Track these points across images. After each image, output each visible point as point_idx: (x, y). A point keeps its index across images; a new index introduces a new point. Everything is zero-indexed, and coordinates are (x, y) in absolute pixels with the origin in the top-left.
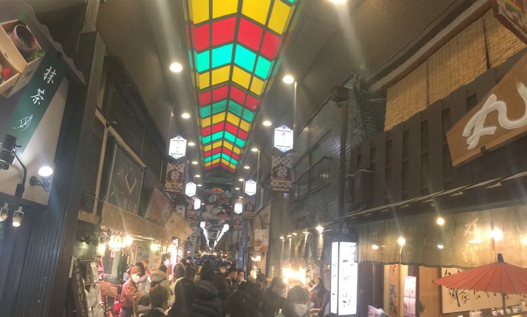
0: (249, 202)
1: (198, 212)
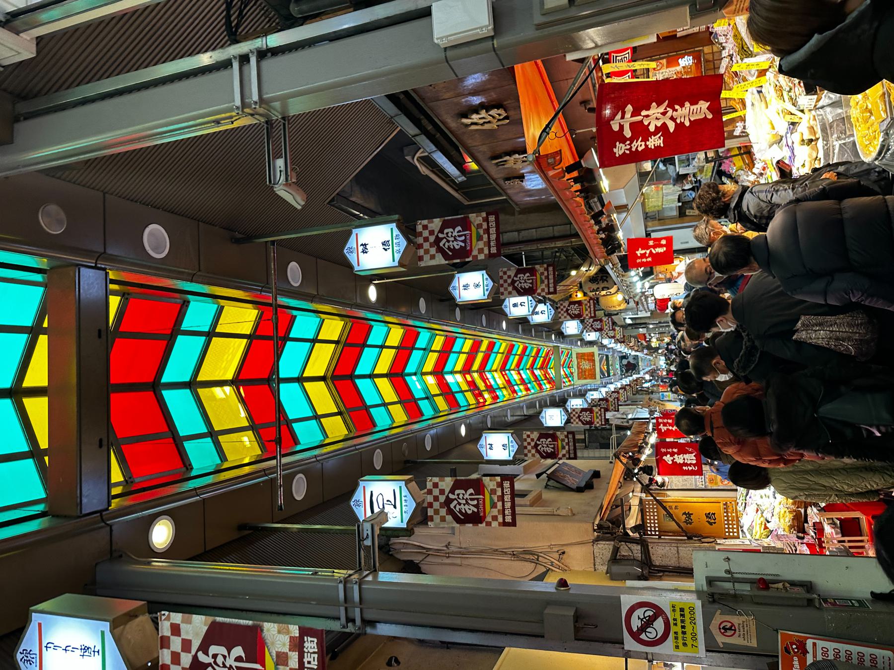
0: (442, 505)
1: (525, 436)
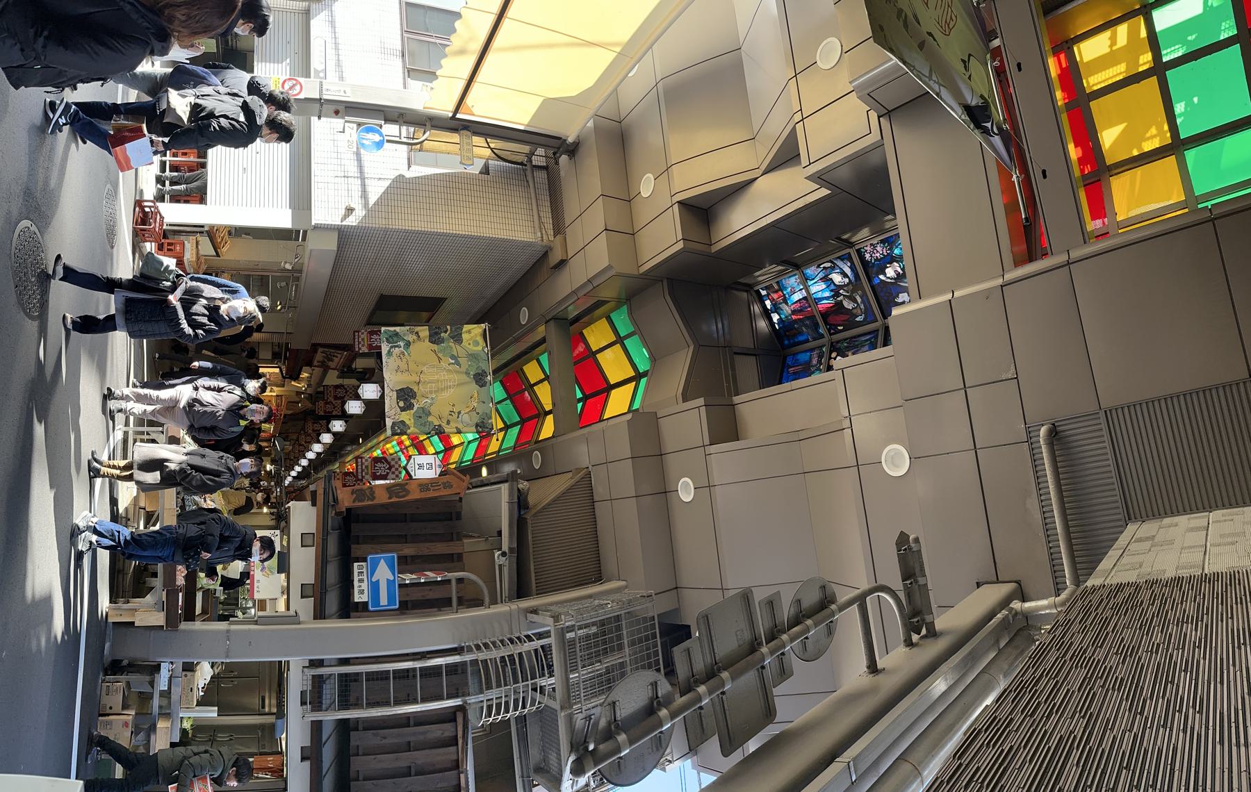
0: (394, 466)
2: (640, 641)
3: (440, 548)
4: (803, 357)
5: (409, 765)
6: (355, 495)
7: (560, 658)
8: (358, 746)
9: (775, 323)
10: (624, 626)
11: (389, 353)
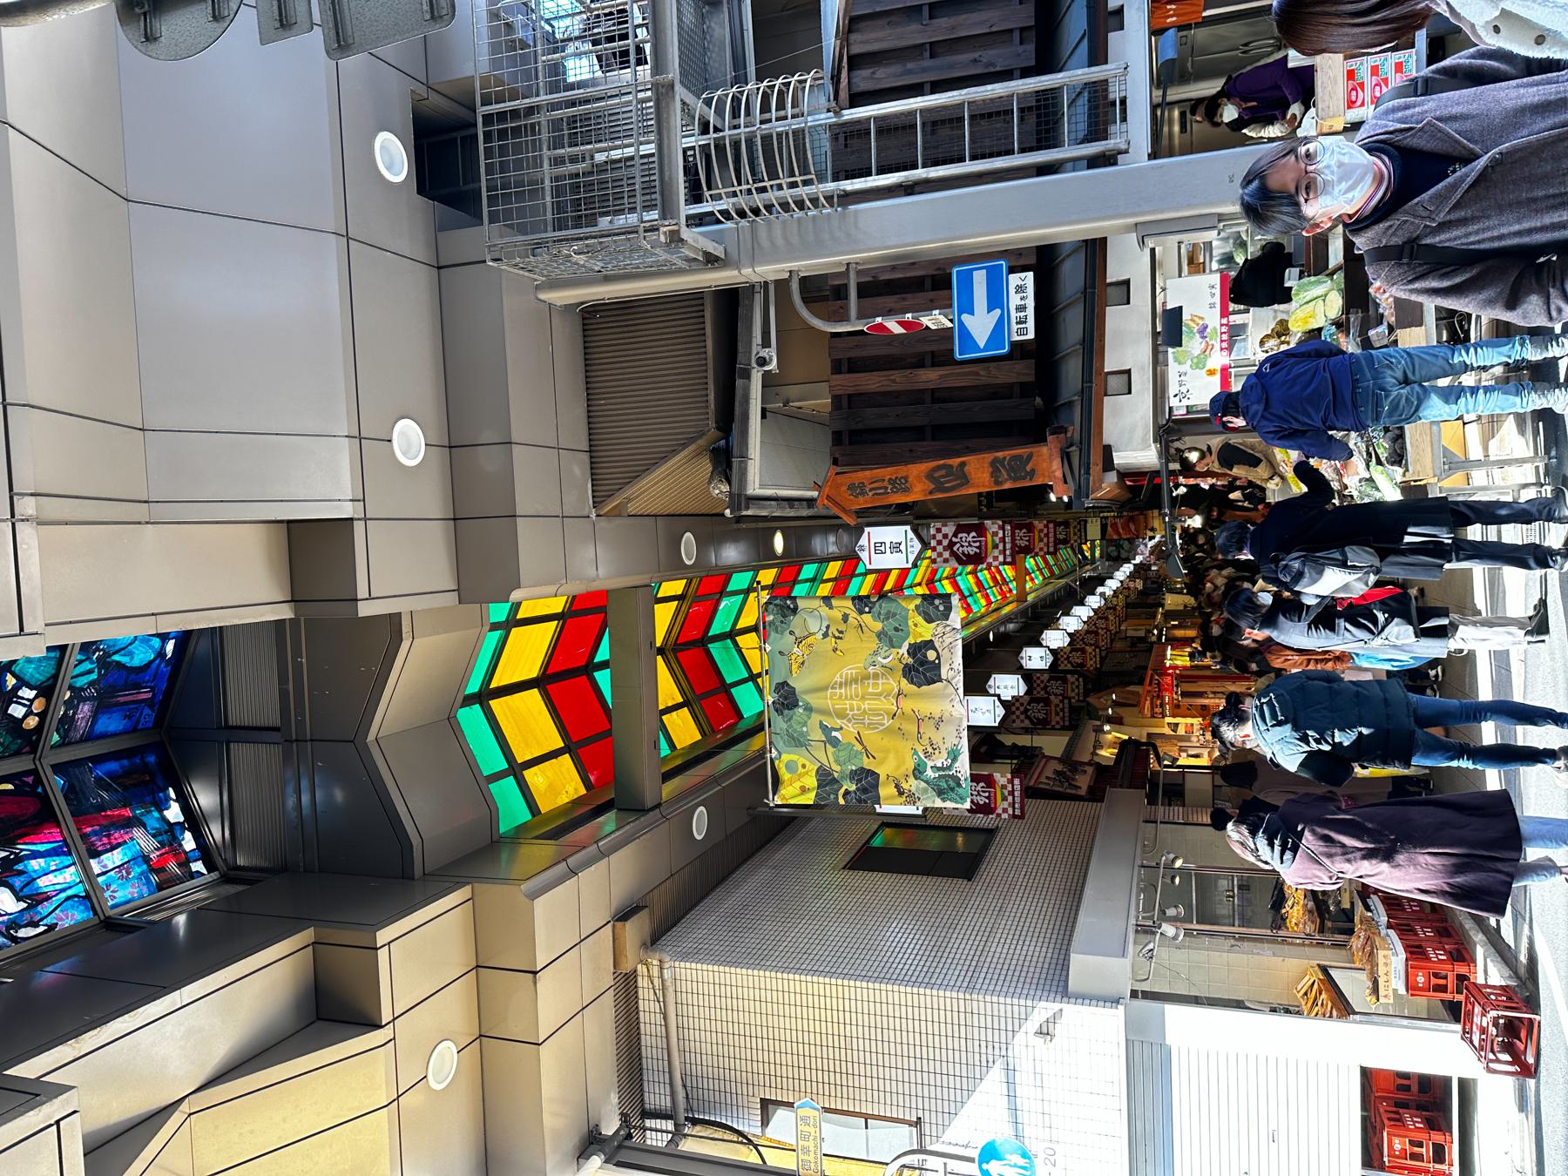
2: (520, 196)
3: (872, 382)
4: (111, 723)
5: (934, 21)
6: (1028, 468)
7: (670, 169)
8: (1021, 43)
9: (175, 801)
10: (548, 193)
11: (954, 755)
